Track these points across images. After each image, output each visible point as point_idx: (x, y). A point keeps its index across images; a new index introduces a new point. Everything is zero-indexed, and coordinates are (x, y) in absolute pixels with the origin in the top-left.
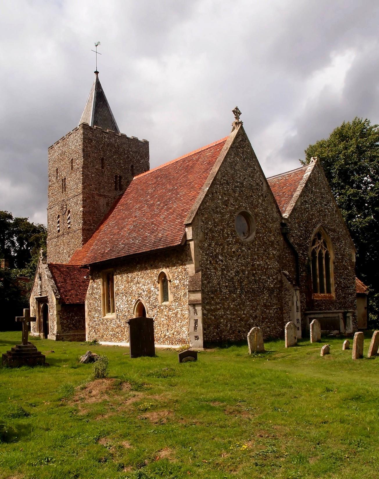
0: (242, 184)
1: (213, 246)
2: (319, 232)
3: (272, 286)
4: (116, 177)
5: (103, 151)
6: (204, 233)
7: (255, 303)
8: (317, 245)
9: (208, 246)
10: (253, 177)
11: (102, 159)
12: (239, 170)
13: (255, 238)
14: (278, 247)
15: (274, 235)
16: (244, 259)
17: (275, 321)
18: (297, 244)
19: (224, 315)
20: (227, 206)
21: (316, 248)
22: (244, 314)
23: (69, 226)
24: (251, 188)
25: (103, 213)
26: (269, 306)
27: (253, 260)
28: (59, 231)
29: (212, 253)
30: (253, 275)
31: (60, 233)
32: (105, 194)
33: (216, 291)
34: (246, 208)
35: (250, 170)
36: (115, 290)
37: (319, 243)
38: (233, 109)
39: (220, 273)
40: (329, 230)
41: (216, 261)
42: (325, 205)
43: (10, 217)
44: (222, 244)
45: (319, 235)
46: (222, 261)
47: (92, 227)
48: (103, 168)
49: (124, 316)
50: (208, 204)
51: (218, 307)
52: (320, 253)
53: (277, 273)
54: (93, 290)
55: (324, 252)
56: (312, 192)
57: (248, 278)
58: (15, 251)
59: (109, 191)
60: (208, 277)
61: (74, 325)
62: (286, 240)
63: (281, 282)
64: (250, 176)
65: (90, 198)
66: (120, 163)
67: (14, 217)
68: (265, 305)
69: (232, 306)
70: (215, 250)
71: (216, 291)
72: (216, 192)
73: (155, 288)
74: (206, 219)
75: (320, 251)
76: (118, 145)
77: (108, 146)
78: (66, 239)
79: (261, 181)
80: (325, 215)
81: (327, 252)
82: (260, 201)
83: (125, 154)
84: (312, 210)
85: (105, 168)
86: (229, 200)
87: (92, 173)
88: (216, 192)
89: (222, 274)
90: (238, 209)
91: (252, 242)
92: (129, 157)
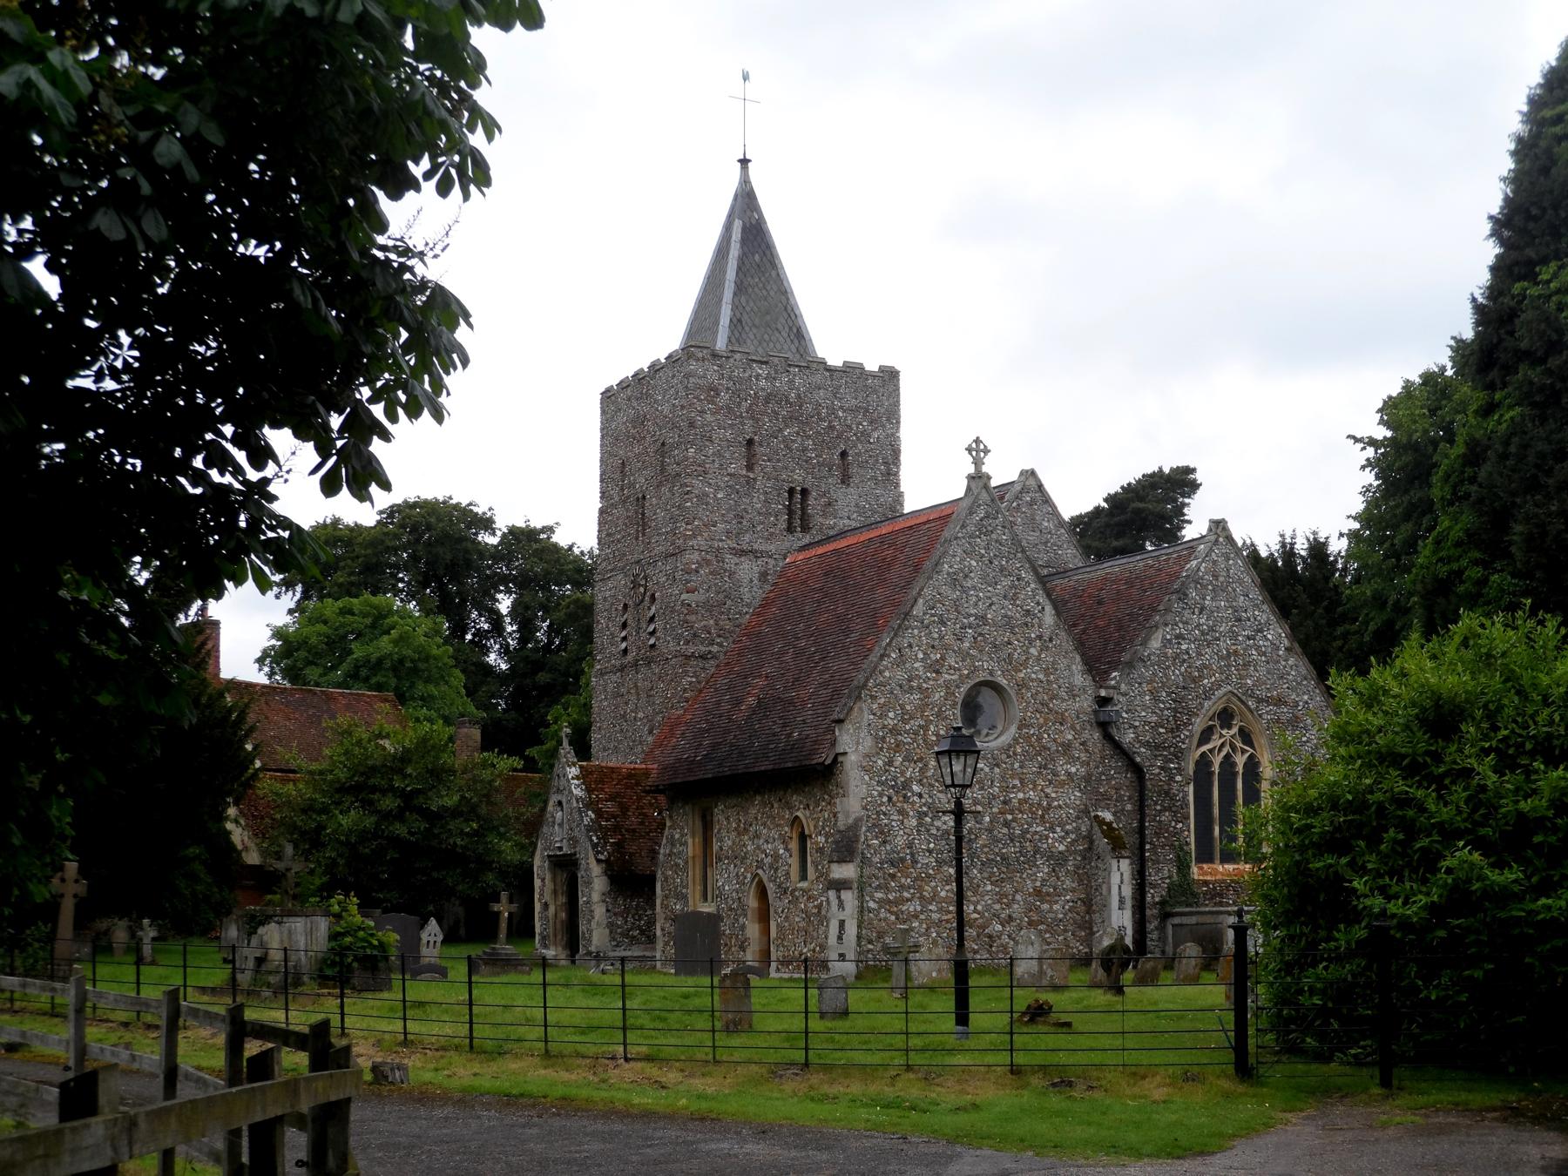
0: (984, 617)
1: (897, 763)
2: (1225, 710)
3: (1062, 848)
4: (791, 491)
5: (752, 418)
6: (876, 737)
7: (1008, 888)
8: (1215, 742)
9: (885, 764)
10: (1015, 598)
11: (750, 442)
12: (974, 588)
13: (1015, 739)
14: (1084, 757)
15: (1073, 728)
16: (982, 789)
17: (1065, 931)
18: (1147, 744)
19: (922, 912)
20: (937, 672)
21: (1211, 751)
22: (975, 911)
23: (652, 641)
24: (1008, 623)
25: (748, 605)
26: (1048, 894)
27: (1006, 789)
28: (625, 651)
29: (895, 779)
30: (1007, 824)
31: (630, 657)
32: (756, 547)
33: (903, 860)
34: (991, 674)
35: (1006, 582)
36: (715, 848)
37: (1221, 736)
38: (969, 440)
39: (914, 822)
40: (1259, 700)
41: (905, 796)
42: (1249, 638)
43: (487, 523)
44: (921, 759)
45: (1225, 717)
46: (920, 796)
47: (715, 649)
48: (750, 467)
49: (731, 909)
50: (887, 674)
51: (906, 894)
52: (1228, 762)
53: (1078, 818)
54: (673, 845)
55: (1240, 760)
56: (1202, 610)
57: (990, 831)
58: (505, 651)
59: (770, 537)
60: (882, 832)
61: (642, 932)
62: (1108, 737)
63: (1089, 839)
64: (1005, 597)
65: (708, 563)
66: (805, 450)
67: (502, 523)
68: (1038, 892)
69: (943, 894)
70: (903, 773)
71: (903, 860)
72: (910, 646)
73: (786, 849)
74: (881, 707)
75: (1228, 756)
76: (799, 396)
77: (767, 401)
78: (642, 677)
79: (1038, 603)
80: (1246, 665)
81: (1251, 757)
82: (1033, 651)
83: (821, 420)
84: (1199, 654)
85: (757, 469)
86: (943, 658)
87: (718, 489)
88: (910, 646)
89: (920, 824)
90: (968, 676)
91: (1006, 749)
92: (831, 428)
